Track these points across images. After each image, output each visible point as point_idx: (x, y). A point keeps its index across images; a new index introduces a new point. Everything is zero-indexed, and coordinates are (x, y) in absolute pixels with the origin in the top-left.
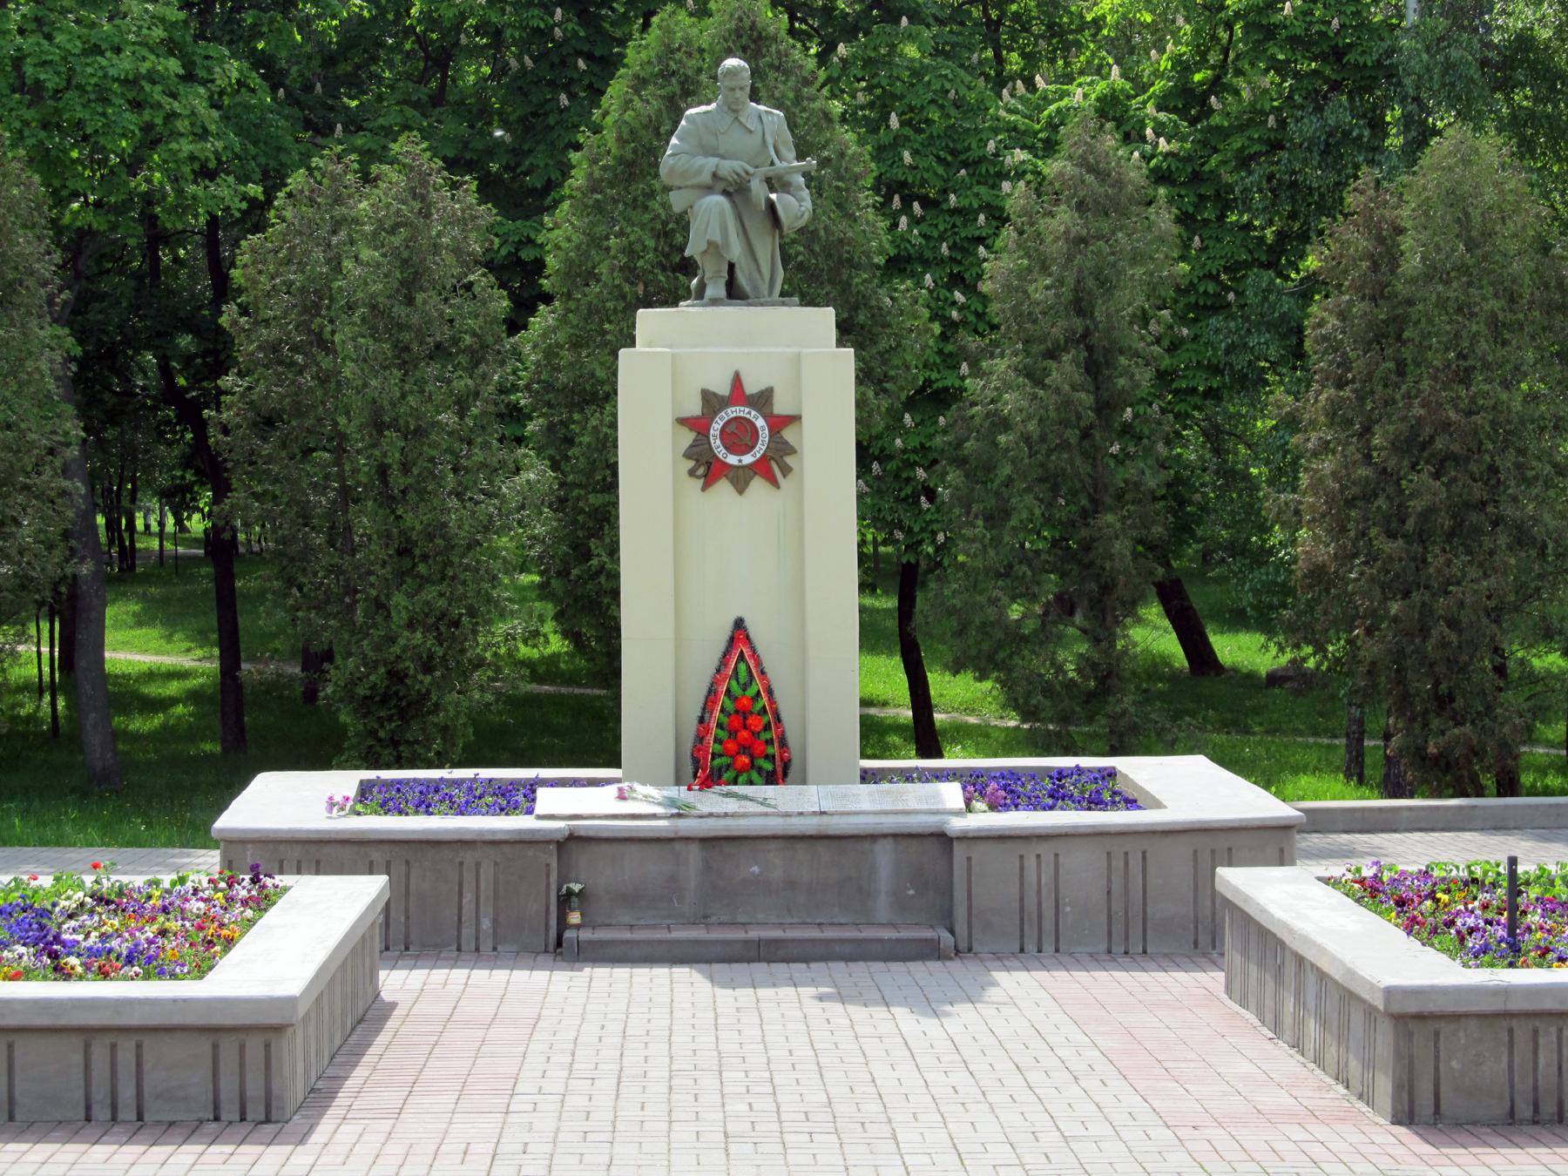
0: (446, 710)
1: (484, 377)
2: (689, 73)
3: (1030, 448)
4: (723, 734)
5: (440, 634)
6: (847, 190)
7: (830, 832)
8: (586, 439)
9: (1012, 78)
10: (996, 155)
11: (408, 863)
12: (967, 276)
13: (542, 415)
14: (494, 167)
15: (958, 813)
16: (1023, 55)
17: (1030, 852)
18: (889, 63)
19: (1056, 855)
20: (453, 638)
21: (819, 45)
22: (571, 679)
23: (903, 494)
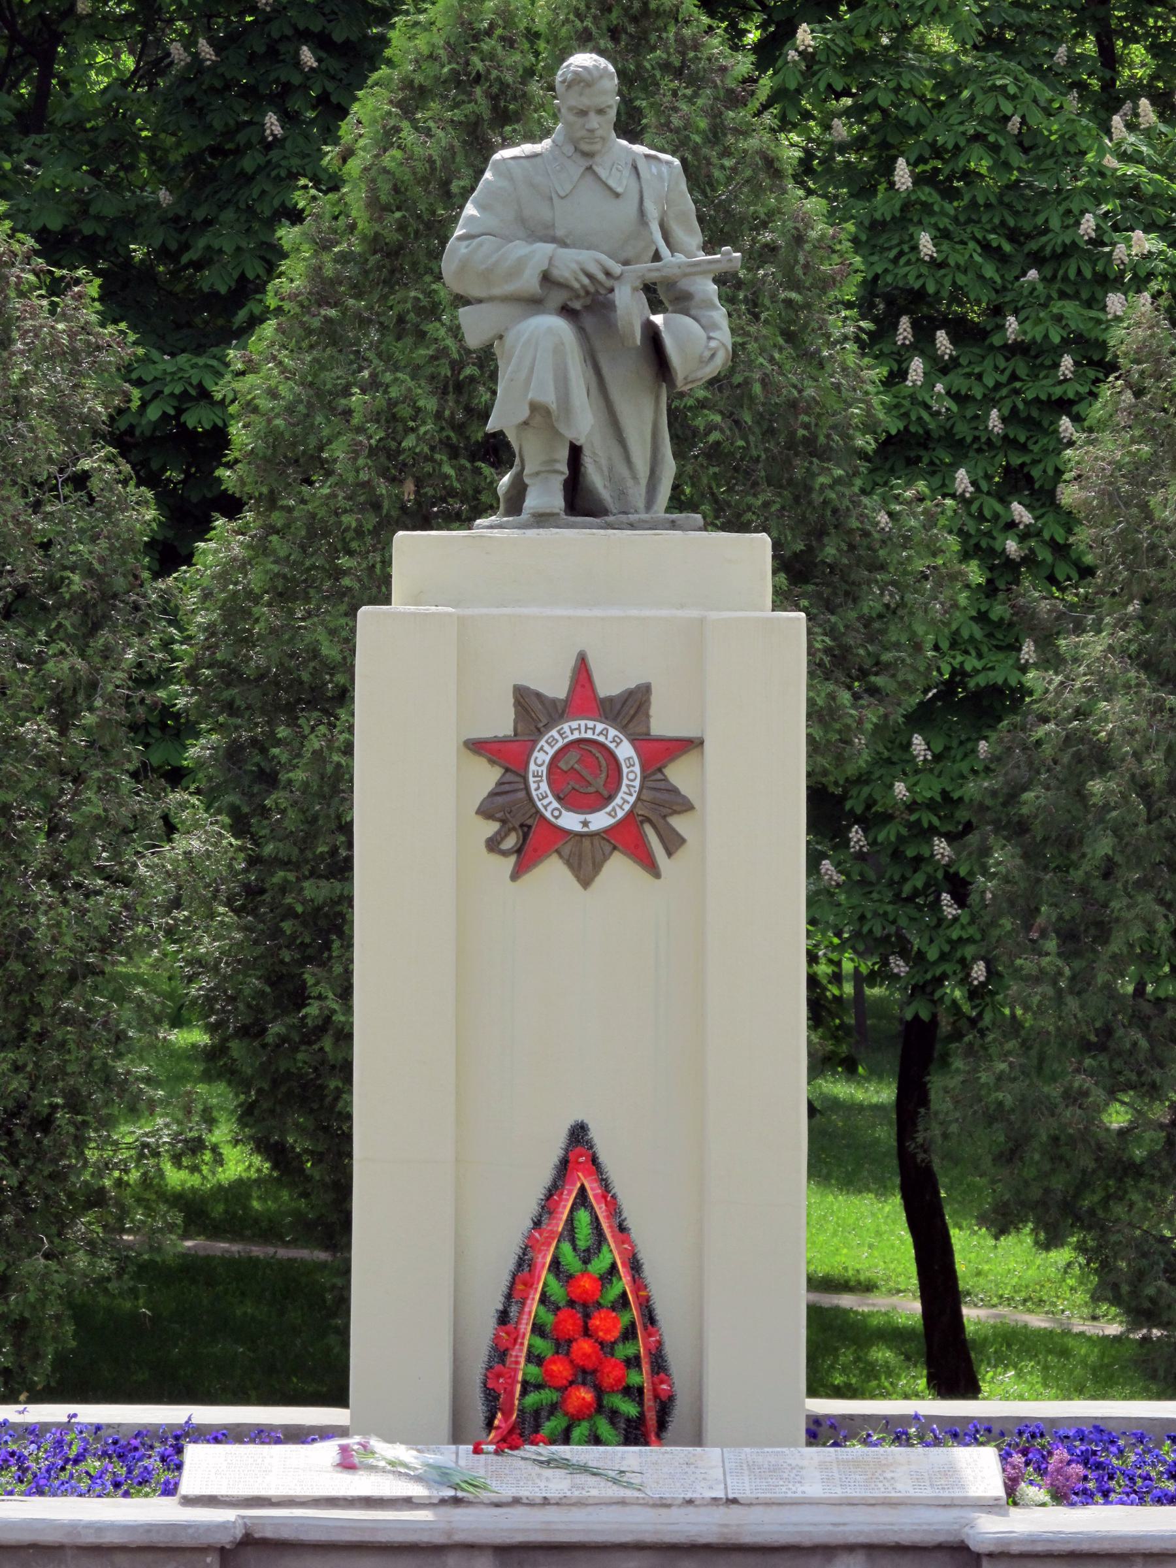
1: (106, 653)
2: (509, 78)
3: (1149, 804)
5: (14, 1144)
6: (808, 306)
7: (747, 1539)
8: (299, 775)
9: (1134, 92)
10: (1098, 242)
12: (1036, 473)
13: (218, 728)
14: (138, 251)
15: (990, 1506)
16: (1156, 50)
18: (896, 63)
21: (763, 26)
22: (267, 1230)
23: (907, 889)
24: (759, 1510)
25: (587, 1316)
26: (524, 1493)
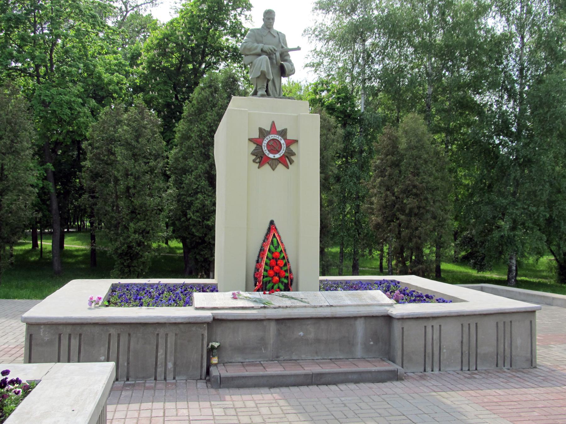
0: (144, 257)
4: (268, 268)
7: (338, 316)
11: (129, 335)
17: (429, 324)
19: (440, 326)
20: (147, 237)
24: (338, 308)
25: (277, 261)
26: (281, 305)
